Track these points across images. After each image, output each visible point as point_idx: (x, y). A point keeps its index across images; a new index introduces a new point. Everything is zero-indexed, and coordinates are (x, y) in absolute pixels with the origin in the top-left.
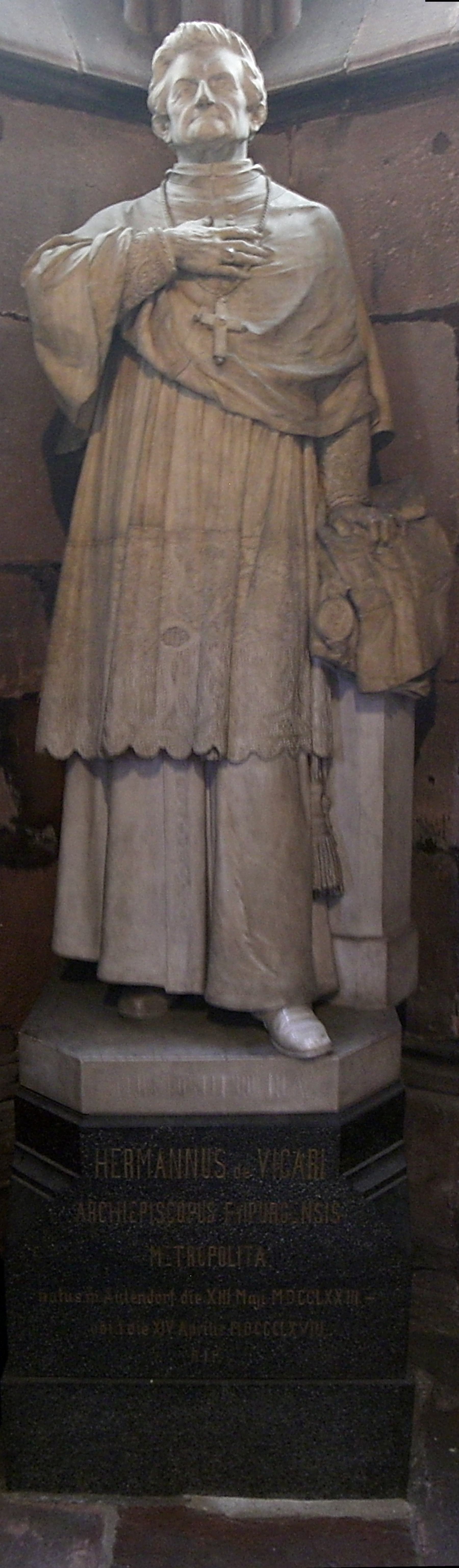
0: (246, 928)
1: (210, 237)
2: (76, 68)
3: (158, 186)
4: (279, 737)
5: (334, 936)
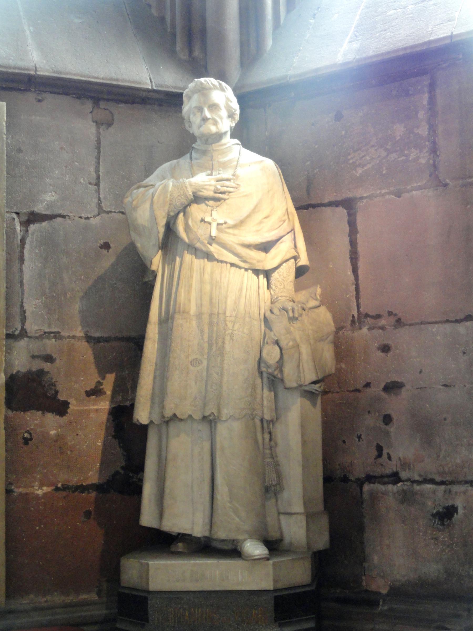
0: (229, 499)
1: (210, 181)
2: (150, 88)
3: (187, 153)
4: (244, 409)
5: (279, 513)
